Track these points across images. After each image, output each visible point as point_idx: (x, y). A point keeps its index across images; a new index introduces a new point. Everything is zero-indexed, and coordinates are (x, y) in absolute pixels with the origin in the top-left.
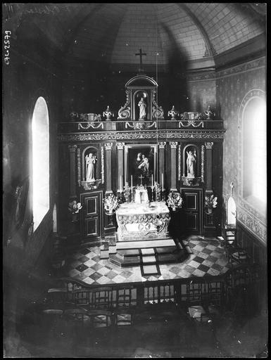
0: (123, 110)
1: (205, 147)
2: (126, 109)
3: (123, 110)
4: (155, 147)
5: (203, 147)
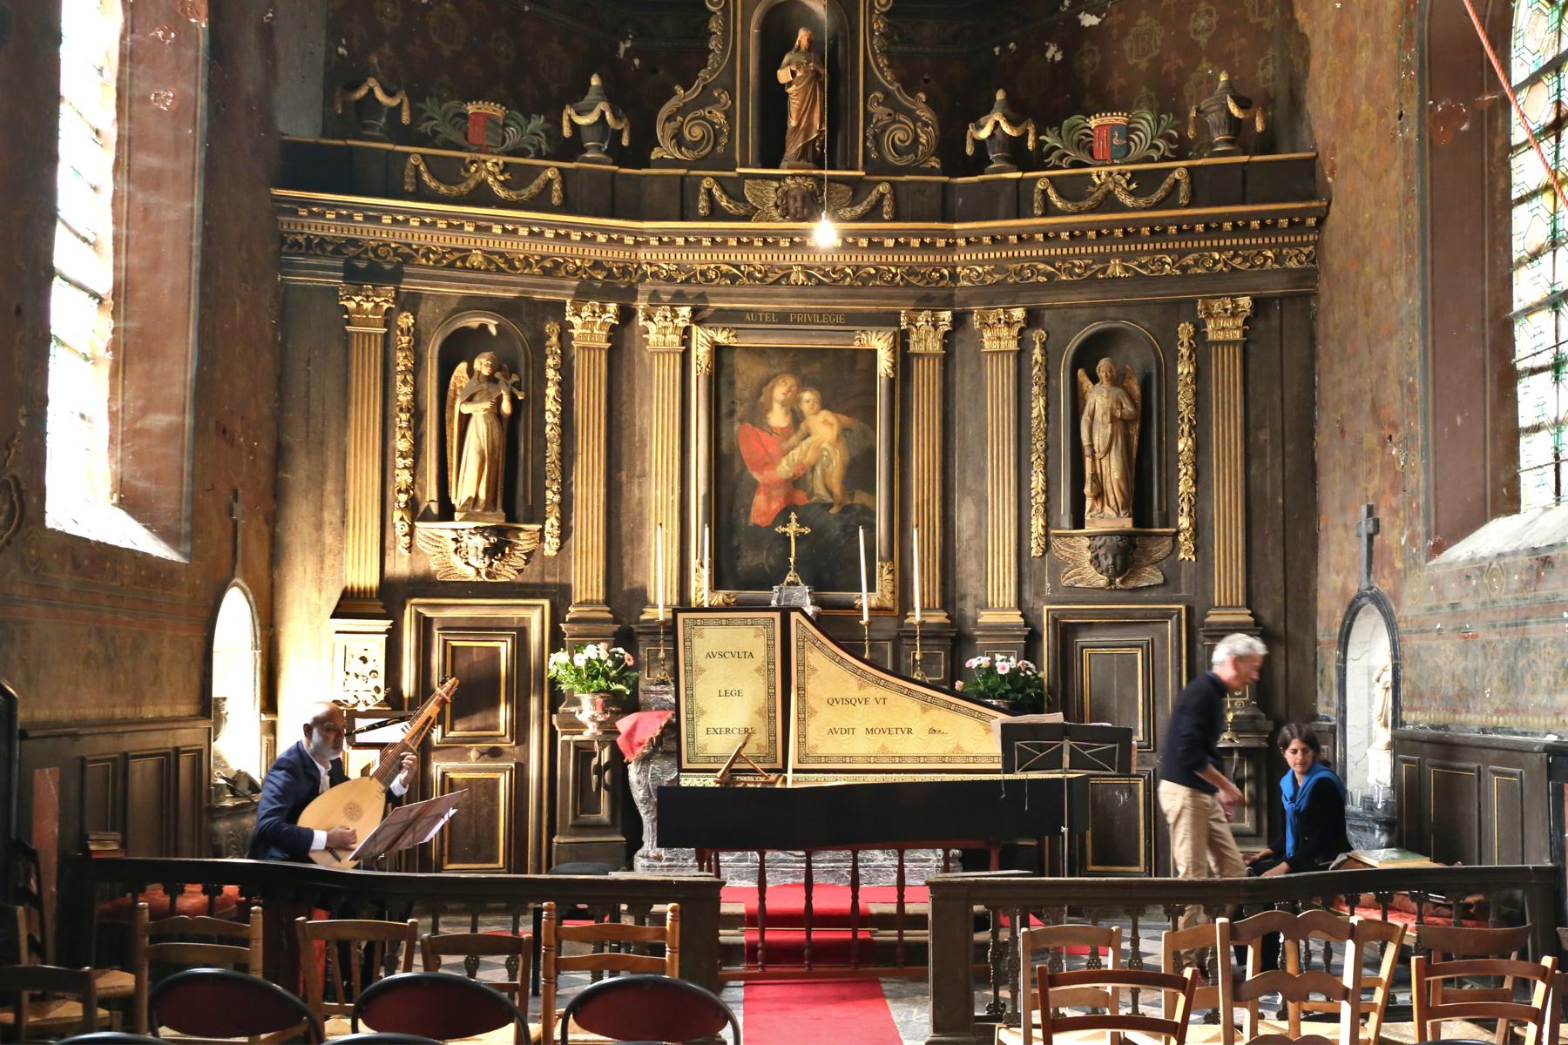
0: (683, 110)
2: (705, 99)
4: (880, 343)
5: (1185, 330)
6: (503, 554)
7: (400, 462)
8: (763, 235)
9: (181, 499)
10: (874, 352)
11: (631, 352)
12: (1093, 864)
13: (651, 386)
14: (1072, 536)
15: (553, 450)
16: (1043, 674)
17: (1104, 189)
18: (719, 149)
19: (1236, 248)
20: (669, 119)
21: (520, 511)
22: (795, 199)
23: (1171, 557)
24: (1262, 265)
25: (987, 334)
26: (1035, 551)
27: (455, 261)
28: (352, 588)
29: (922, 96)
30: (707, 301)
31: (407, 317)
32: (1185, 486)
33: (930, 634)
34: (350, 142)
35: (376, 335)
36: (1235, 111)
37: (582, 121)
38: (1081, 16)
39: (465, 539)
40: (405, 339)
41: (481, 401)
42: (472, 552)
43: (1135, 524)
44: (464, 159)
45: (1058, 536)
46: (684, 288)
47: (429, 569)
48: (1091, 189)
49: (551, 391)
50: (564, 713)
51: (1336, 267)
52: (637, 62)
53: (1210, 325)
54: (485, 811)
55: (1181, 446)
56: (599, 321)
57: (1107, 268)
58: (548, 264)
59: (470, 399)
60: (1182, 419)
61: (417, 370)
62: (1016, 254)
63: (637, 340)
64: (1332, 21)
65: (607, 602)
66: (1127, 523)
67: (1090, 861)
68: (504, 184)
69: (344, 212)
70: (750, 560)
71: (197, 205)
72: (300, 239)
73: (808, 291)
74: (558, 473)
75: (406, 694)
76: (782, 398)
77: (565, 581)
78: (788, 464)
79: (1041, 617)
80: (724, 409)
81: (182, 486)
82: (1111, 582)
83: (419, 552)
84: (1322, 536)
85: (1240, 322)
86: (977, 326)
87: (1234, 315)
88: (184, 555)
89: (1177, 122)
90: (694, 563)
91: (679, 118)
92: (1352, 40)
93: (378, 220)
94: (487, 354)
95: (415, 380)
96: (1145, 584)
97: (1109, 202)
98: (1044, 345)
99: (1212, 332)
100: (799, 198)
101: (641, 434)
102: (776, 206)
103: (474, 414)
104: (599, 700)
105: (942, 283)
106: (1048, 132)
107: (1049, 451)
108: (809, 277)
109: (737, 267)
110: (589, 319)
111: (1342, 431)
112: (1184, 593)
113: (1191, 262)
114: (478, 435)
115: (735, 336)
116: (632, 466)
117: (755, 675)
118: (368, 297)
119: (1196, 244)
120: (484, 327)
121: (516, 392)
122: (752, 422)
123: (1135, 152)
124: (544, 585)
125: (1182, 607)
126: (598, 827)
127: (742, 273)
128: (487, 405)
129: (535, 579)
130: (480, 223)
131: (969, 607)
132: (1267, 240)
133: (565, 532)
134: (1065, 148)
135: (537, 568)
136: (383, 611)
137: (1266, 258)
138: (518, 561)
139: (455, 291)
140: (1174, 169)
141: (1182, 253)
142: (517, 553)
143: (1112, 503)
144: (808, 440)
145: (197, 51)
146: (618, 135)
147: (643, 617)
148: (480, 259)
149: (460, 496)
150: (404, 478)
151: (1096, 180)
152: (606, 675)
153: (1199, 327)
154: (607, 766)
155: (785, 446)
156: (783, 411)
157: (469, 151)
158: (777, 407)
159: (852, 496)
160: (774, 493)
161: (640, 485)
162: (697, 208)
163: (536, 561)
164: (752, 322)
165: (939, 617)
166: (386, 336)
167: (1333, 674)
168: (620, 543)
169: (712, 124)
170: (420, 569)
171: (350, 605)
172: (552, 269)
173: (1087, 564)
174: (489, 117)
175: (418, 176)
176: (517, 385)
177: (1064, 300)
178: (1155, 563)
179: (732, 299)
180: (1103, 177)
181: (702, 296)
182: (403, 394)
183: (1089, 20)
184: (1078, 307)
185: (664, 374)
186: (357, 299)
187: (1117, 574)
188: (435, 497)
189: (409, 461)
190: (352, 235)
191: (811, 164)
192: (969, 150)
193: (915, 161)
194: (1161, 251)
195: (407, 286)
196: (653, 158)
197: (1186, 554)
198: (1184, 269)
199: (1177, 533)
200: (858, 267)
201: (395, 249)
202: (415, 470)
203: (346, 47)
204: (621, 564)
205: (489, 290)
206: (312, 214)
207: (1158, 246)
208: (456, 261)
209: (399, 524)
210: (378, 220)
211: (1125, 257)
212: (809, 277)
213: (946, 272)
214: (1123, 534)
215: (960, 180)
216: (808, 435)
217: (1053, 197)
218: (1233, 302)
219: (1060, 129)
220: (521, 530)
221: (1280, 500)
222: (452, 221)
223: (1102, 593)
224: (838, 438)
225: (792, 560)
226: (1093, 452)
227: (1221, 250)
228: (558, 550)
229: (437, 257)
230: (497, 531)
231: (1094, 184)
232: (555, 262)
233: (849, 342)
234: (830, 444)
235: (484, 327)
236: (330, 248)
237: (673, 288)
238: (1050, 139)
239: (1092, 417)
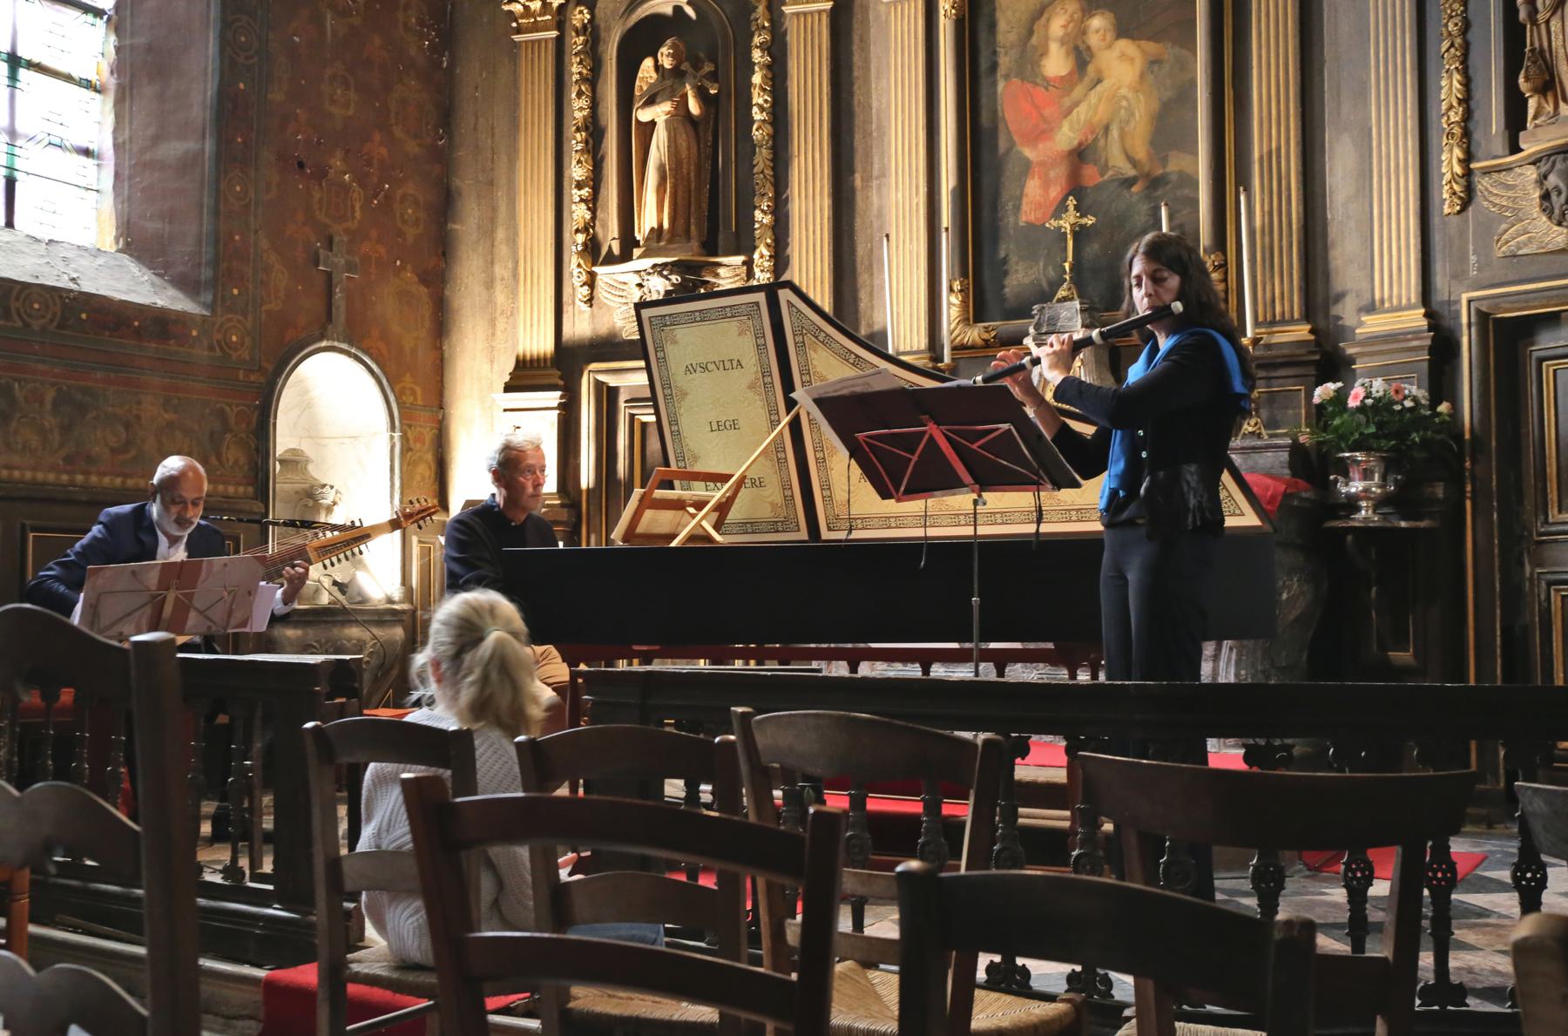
7: (576, 194)
9: (200, 241)
13: (887, 49)
15: (762, 157)
28: (524, 356)
31: (581, 12)
35: (546, 40)
45: (1487, 172)
47: (614, 327)
61: (593, 79)
74: (768, 185)
75: (584, 485)
78: (1071, 129)
79: (1458, 314)
80: (984, 64)
81: (201, 225)
88: (205, 306)
95: (594, 91)
101: (879, 119)
117: (750, 394)
121: (707, 83)
122: (1021, 75)
131: (1346, 311)
136: (561, 383)
144: (1099, 88)
150: (579, 213)
155: (1067, 102)
156: (1063, 51)
158: (1054, 48)
159: (1164, 161)
160: (1052, 174)
161: (879, 187)
170: (603, 329)
171: (525, 376)
176: (713, 77)
182: (578, 108)
188: (616, 236)
189: (585, 192)
202: (593, 203)
216: (1099, 81)
220: (719, 265)
224: (1142, 76)
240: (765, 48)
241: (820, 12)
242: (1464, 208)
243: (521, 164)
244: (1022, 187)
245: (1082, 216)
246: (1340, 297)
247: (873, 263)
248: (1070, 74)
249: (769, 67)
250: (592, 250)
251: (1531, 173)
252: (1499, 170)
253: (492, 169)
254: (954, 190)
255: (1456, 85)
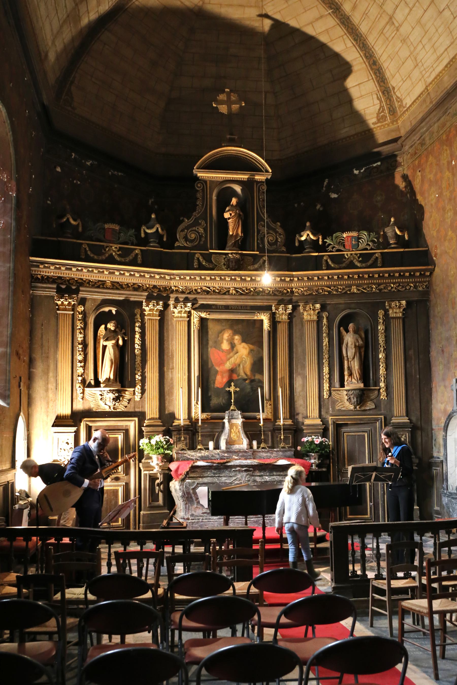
0: (187, 228)
1: (386, 314)
2: (196, 223)
3: (187, 228)
4: (265, 318)
5: (381, 313)
6: (120, 400)
7: (79, 364)
8: (220, 276)
10: (262, 321)
11: (168, 320)
12: (350, 515)
14: (339, 390)
15: (138, 359)
16: (330, 443)
17: (349, 260)
18: (202, 243)
19: (399, 283)
20: (182, 231)
21: (127, 383)
22: (232, 262)
23: (378, 398)
24: (409, 289)
25: (305, 314)
26: (326, 396)
27: (100, 285)
28: (60, 415)
29: (279, 224)
30: (197, 301)
31: (81, 307)
32: (382, 371)
33: (286, 429)
34: (59, 239)
35: (69, 314)
36: (398, 233)
37: (149, 231)
38: (330, 194)
39: (105, 394)
40: (80, 316)
41: (111, 340)
42: (108, 400)
43: (364, 386)
44: (103, 246)
45: (334, 390)
46: (189, 296)
48: (344, 260)
49: (137, 336)
50: (145, 463)
51: (438, 290)
52: (156, 207)
53: (391, 311)
54: (113, 502)
55: (380, 356)
56: (183, 310)
57: (351, 289)
58: (136, 286)
59: (107, 340)
60: (381, 346)
62: (316, 284)
63: (170, 316)
64: (434, 201)
65: (160, 418)
66: (361, 385)
67: (348, 514)
68: (119, 255)
69: (58, 266)
70: (215, 401)
71: (12, 265)
72: (39, 276)
73: (236, 297)
74: (140, 368)
76: (227, 338)
77: (143, 410)
78: (229, 364)
79: (328, 421)
82: (355, 408)
83: (86, 400)
84: (434, 390)
85: (401, 310)
86: (302, 311)
87: (400, 307)
89: (377, 236)
90: (193, 402)
91: (186, 231)
92: (444, 209)
93: (71, 269)
94: (113, 322)
95: (84, 332)
96: (368, 408)
97: (351, 265)
98: (327, 318)
99: (391, 313)
100: (234, 262)
102: (224, 265)
103: (108, 345)
104: (160, 457)
105: (288, 294)
106: (327, 238)
107: (330, 358)
108: (237, 292)
109: (209, 288)
110: (152, 308)
111: (443, 351)
112: (382, 412)
113: (383, 288)
114: (110, 353)
115: (209, 314)
116: (168, 364)
118: (66, 299)
119: (385, 281)
120: (110, 311)
122: (215, 347)
123: (361, 246)
124: (135, 412)
125: (383, 417)
126: (159, 507)
127: (211, 290)
128: (113, 342)
129: (132, 410)
130: (110, 271)
131: (300, 418)
132: (411, 280)
133: (143, 391)
134: (334, 244)
135: (132, 405)
136: (73, 424)
137: (411, 287)
138: (125, 403)
139: (100, 297)
140: (375, 253)
141: (379, 285)
142: (125, 400)
143: (355, 378)
144: (237, 354)
145: (12, 205)
146: (162, 236)
147: (174, 424)
148: (110, 284)
149: (102, 379)
150: (80, 371)
151: (346, 257)
152: (163, 447)
153: (386, 311)
154: (161, 483)
155: (228, 356)
156: (227, 343)
157: (106, 243)
159: (254, 376)
160: (224, 375)
161: (172, 372)
162: (194, 265)
163: (132, 402)
164: (215, 309)
165: (289, 422)
166: (73, 314)
167: (441, 442)
168: (164, 395)
169: (199, 233)
170: (86, 407)
172: (137, 288)
173: (346, 401)
174: (113, 230)
175: (86, 251)
176: (125, 334)
177: (335, 301)
178: (371, 400)
179: (207, 300)
180: (349, 255)
181: (195, 299)
182: (80, 337)
183: (334, 196)
184: (340, 304)
185: (181, 329)
186: (62, 300)
187: (358, 405)
188: (93, 378)
189: (82, 364)
190: (60, 275)
191: (238, 249)
192: (297, 244)
193: (276, 248)
194: (372, 283)
195: (81, 295)
196: (176, 245)
197: (383, 396)
198: (380, 290)
199: (379, 389)
200: (255, 288)
201: (76, 281)
202: (84, 367)
203: (50, 201)
204: (164, 403)
205: (113, 296)
206: (45, 267)
207: (370, 281)
208: (100, 285)
209: (78, 389)
210: (71, 269)
211: (358, 286)
212: (237, 292)
213: (289, 290)
214: (360, 390)
215: (294, 255)
216: (237, 353)
217: (330, 263)
218: (399, 303)
219: (332, 237)
220: (126, 390)
221: (418, 376)
222: (99, 270)
223: (352, 412)
224: (249, 353)
225: (232, 401)
226: (348, 359)
227: (394, 283)
228: (141, 398)
229: (93, 284)
230: (118, 391)
231: (345, 258)
232: (139, 286)
233: (253, 317)
234: (245, 355)
235: (110, 311)
236: (51, 280)
237: (184, 296)
238: (328, 241)
239: (347, 345)
240: (139, 327)
241: (156, 320)
242: (329, 396)
243: (59, 353)
244: (216, 377)
245: (236, 388)
246: (298, 414)
247: (171, 393)
248: (229, 349)
249: (140, 333)
250: (83, 382)
251: (345, 393)
252: (337, 390)
253: (48, 353)
254: (198, 377)
255: (327, 369)
